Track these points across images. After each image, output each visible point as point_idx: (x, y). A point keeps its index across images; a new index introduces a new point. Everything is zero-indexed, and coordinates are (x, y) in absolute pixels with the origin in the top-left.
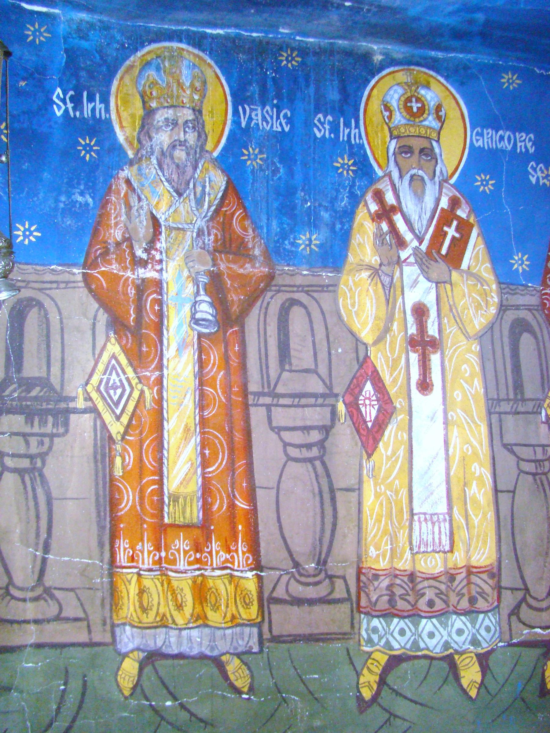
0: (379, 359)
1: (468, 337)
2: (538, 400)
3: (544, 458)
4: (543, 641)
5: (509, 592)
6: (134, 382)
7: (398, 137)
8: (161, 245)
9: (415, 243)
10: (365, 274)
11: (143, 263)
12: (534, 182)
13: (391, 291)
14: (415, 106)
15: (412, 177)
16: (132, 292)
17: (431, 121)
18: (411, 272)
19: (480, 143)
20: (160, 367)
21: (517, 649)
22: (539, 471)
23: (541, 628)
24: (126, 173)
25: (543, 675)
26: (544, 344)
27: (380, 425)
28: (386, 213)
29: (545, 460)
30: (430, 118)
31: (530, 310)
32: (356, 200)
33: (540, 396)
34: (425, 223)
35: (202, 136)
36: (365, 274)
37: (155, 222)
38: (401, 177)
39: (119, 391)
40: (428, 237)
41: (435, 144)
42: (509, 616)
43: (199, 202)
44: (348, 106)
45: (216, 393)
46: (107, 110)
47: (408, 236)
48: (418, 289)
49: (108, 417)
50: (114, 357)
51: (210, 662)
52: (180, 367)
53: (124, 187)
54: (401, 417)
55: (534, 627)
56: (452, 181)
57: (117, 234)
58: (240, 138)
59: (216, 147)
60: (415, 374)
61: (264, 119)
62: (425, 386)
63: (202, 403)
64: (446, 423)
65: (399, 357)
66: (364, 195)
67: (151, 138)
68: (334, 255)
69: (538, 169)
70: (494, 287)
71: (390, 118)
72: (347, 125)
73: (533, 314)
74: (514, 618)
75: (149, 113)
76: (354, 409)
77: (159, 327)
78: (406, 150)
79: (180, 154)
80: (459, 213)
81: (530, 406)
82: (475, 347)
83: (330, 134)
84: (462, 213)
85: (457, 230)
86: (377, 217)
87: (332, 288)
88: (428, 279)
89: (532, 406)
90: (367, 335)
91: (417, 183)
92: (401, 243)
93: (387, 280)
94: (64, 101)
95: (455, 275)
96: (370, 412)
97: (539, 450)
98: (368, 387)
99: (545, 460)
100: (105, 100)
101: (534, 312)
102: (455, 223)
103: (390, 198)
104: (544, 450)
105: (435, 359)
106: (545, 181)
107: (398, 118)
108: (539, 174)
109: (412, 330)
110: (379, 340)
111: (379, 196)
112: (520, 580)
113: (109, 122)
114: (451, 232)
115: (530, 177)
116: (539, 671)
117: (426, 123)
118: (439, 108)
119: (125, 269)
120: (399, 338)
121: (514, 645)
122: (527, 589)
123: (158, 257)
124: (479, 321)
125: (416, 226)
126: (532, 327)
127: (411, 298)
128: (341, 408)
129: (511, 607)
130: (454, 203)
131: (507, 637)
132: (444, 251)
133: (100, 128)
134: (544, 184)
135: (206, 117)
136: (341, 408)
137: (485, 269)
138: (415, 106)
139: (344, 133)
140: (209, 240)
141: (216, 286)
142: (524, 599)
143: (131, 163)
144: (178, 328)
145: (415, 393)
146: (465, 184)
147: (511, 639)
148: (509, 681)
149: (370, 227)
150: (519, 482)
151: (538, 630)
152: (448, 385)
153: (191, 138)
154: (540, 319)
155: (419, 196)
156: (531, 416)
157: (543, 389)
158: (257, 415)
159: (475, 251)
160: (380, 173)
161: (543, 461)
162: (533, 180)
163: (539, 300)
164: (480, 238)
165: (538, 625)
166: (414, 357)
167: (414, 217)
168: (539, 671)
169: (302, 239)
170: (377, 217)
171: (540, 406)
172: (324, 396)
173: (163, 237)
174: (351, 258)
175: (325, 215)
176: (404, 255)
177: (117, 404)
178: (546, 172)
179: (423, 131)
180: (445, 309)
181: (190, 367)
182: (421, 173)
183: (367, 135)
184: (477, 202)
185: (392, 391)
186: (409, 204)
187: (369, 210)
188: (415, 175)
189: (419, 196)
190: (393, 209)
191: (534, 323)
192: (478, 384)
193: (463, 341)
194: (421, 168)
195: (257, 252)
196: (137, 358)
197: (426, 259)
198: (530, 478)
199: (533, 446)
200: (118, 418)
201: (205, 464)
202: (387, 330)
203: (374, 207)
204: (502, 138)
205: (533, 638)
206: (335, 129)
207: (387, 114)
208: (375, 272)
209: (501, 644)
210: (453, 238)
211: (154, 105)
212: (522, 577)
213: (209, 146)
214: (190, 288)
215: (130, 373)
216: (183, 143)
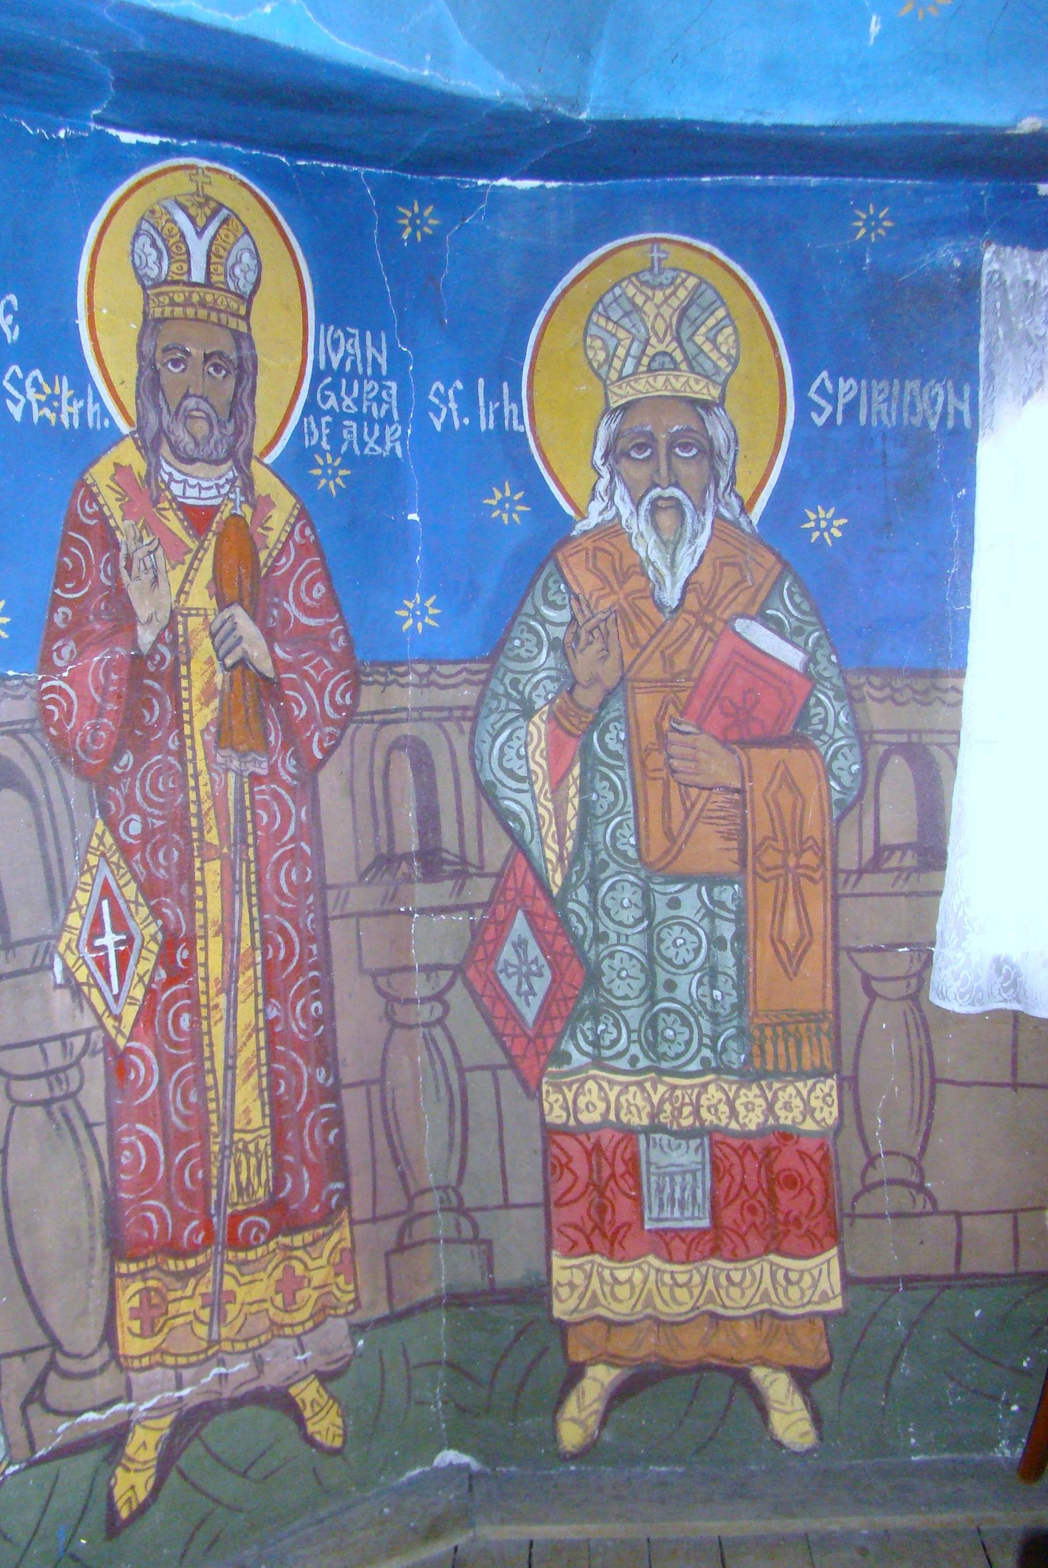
2: (41, 939)
3: (68, 1062)
4: (99, 1435)
5: (17, 1361)
12: (18, 417)
15: (653, 503)
21: (45, 1467)
22: (58, 1093)
23: (95, 1409)
25: (110, 1496)
26: (50, 809)
29: (70, 1066)
31: (14, 734)
33: (46, 928)
42: (24, 1408)
55: (80, 1413)
69: (28, 383)
72: (493, 394)
73: (21, 742)
74: (34, 1409)
81: (26, 955)
83: (461, 418)
89: (30, 957)
91: (666, 519)
97: (54, 1049)
99: (70, 1066)
101: (26, 737)
104: (64, 1045)
105: (384, 850)
106: (46, 411)
108: (31, 394)
112: (39, 1331)
115: (9, 403)
116: (101, 1491)
121: (43, 1460)
122: (55, 1344)
126: (20, 773)
129: (26, 1390)
131: (23, 1452)
134: (44, 419)
142: (52, 1365)
147: (33, 1449)
148: (41, 1532)
150: (15, 1126)
151: (91, 1416)
154: (39, 752)
156: (29, 978)
157: (55, 913)
161: (65, 1069)
162: (16, 412)
163: (35, 706)
165: (89, 1405)
168: (101, 1491)
171: (49, 952)
178: (47, 390)
182: (678, 493)
183: (532, 418)
188: (660, 498)
191: (24, 763)
198: (39, 1112)
199: (40, 1042)
205: (80, 1435)
209: (12, 1469)
212: (42, 1322)
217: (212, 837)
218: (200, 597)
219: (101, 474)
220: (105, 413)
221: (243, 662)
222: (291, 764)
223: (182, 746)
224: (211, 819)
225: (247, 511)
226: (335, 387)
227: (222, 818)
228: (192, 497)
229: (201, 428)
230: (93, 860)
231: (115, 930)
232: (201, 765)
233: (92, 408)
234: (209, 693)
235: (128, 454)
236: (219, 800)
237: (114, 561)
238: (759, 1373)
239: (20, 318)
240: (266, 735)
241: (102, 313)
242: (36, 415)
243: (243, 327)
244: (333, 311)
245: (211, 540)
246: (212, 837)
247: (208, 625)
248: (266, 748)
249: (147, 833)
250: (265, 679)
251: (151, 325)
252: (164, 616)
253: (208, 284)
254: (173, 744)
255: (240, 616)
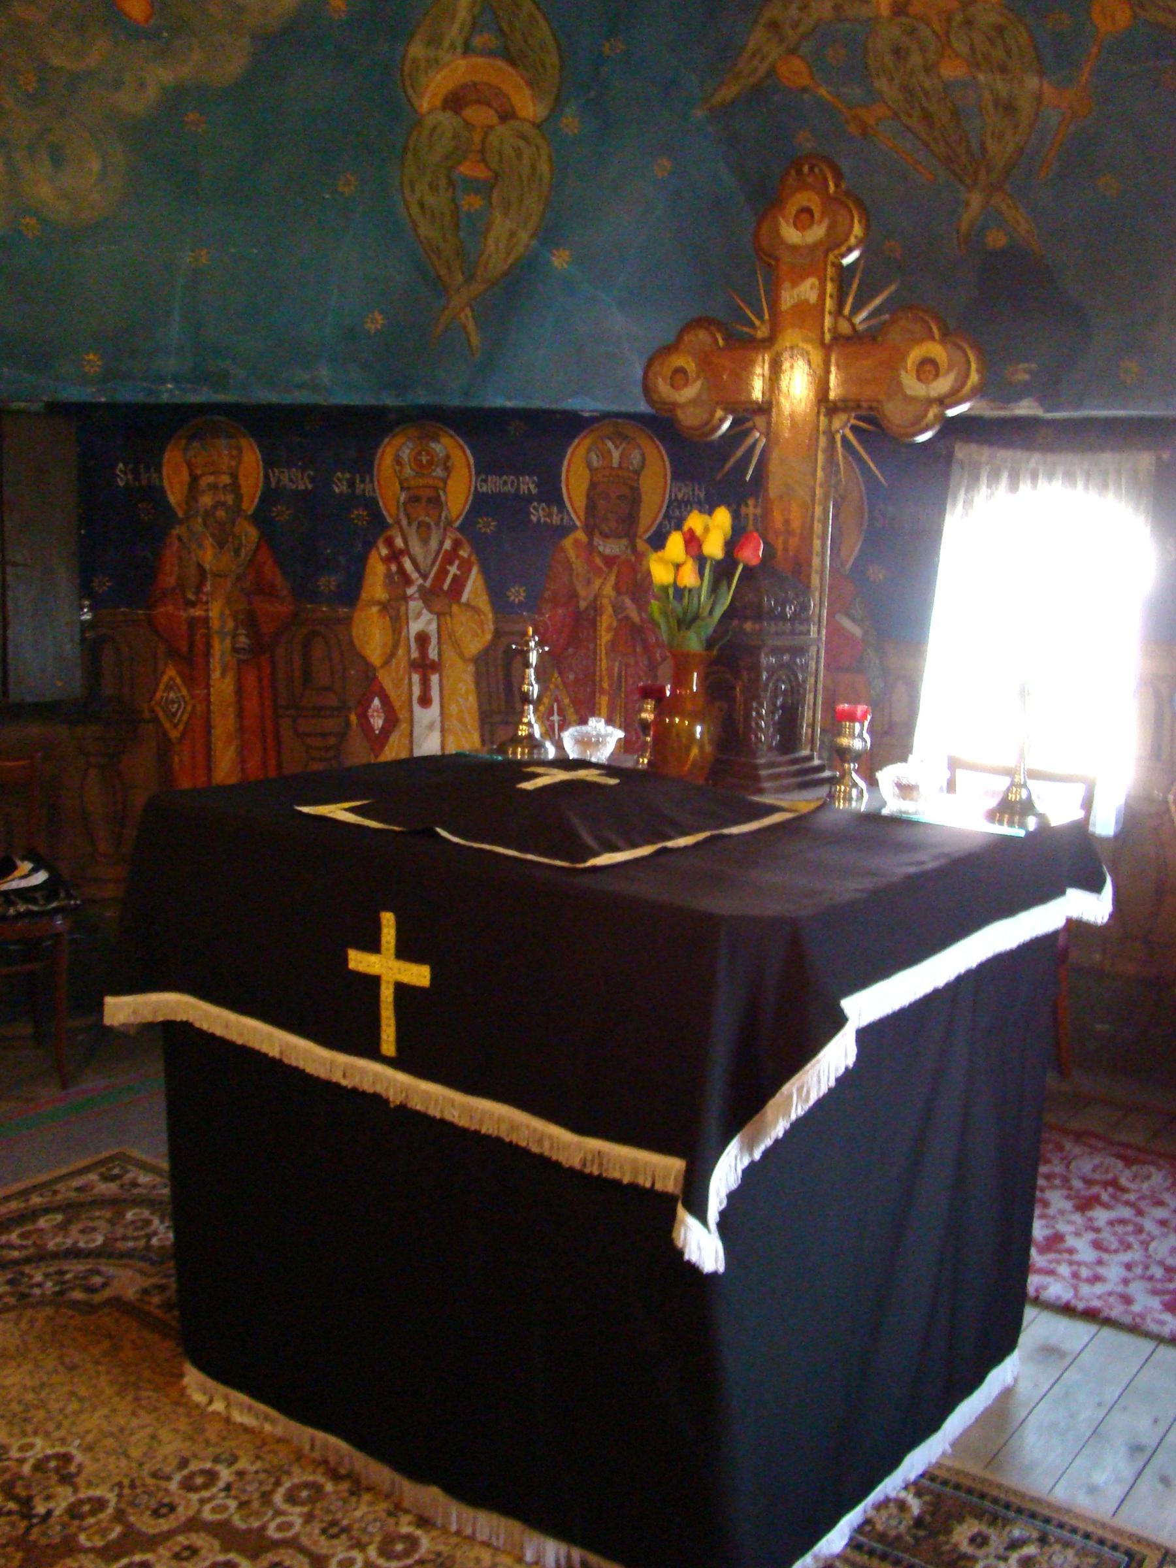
0: (386, 679)
1: (465, 660)
6: (188, 698)
7: (408, 489)
8: (208, 588)
9: (420, 581)
10: (375, 609)
11: (193, 604)
13: (397, 622)
14: (424, 459)
16: (184, 627)
17: (439, 472)
18: (415, 605)
19: (484, 489)
20: (208, 686)
24: (177, 531)
27: (386, 731)
28: (395, 556)
30: (439, 470)
32: (369, 545)
34: (429, 562)
35: (239, 498)
36: (375, 609)
37: (200, 568)
38: (409, 524)
39: (176, 706)
40: (432, 575)
41: (441, 493)
43: (237, 551)
44: (364, 466)
45: (252, 705)
46: (161, 479)
47: (415, 575)
48: (421, 621)
49: (168, 726)
50: (171, 679)
51: (306, 1560)
52: (222, 686)
53: (177, 544)
54: (404, 726)
56: (457, 524)
57: (171, 581)
58: (270, 496)
59: (249, 507)
60: (417, 691)
61: (291, 480)
62: (425, 701)
63: (240, 715)
64: (443, 730)
65: (403, 679)
66: (375, 542)
67: (197, 502)
68: (350, 593)
70: (490, 616)
71: (401, 472)
75: (194, 479)
76: (364, 717)
77: (207, 654)
78: (414, 500)
79: (221, 514)
80: (461, 553)
82: (471, 668)
84: (464, 553)
85: (458, 569)
86: (387, 560)
87: (347, 621)
88: (431, 612)
90: (376, 658)
92: (408, 581)
93: (393, 612)
94: (125, 473)
95: (455, 608)
96: (378, 722)
98: (376, 702)
100: (160, 472)
102: (457, 562)
103: (399, 542)
105: (435, 679)
107: (408, 471)
109: (415, 655)
110: (387, 663)
111: (389, 542)
113: (162, 488)
114: (453, 570)
117: (434, 474)
118: (448, 457)
119: (179, 609)
120: (404, 664)
123: (204, 599)
124: (474, 647)
125: (422, 566)
127: (415, 627)
128: (353, 718)
130: (457, 544)
132: (446, 587)
133: (156, 495)
135: (242, 481)
136: (353, 718)
137: (483, 603)
138: (424, 459)
139: (359, 487)
140: (247, 584)
141: (250, 621)
143: (181, 522)
144: (220, 649)
145: (416, 707)
146: (467, 526)
149: (380, 569)
152: (445, 699)
153: (230, 499)
155: (425, 541)
158: (285, 723)
159: (474, 587)
160: (390, 521)
162: (534, 519)
164: (480, 576)
166: (416, 678)
167: (420, 558)
169: (322, 581)
170: (387, 560)
172: (338, 709)
173: (208, 583)
174: (364, 595)
175: (342, 560)
176: (410, 591)
177: (175, 714)
179: (431, 482)
180: (445, 637)
181: (232, 687)
184: (480, 544)
185: (397, 705)
186: (416, 548)
187: (379, 554)
189: (425, 541)
190: (402, 552)
192: (472, 700)
193: (460, 664)
194: (428, 515)
195: (284, 593)
196: (190, 681)
197: (429, 596)
200: (175, 726)
201: (243, 762)
202: (393, 654)
203: (384, 552)
204: (505, 483)
206: (351, 484)
207: (398, 468)
208: (384, 607)
210: (455, 575)
211: (199, 472)
213: (244, 506)
214: (230, 624)
215: (184, 692)
216: (223, 504)
217: (605, 685)
218: (608, 590)
219: (568, 543)
220: (571, 519)
221: (627, 618)
222: (646, 662)
223: (595, 648)
224: (606, 679)
225: (633, 559)
226: (679, 507)
227: (611, 676)
228: (608, 552)
229: (613, 524)
230: (552, 686)
231: (559, 715)
232: (603, 656)
233: (566, 518)
234: (609, 629)
235: (580, 535)
236: (610, 670)
237: (571, 575)
238: (964, 226)
239: (538, 486)
240: (634, 646)
241: (572, 480)
242: (542, 520)
243: (635, 484)
244: (676, 476)
245: (615, 568)
246: (605, 685)
247: (611, 602)
248: (635, 654)
249: (577, 680)
250: (633, 624)
251: (593, 486)
252: (591, 597)
253: (620, 467)
254: (591, 646)
255: (628, 601)
